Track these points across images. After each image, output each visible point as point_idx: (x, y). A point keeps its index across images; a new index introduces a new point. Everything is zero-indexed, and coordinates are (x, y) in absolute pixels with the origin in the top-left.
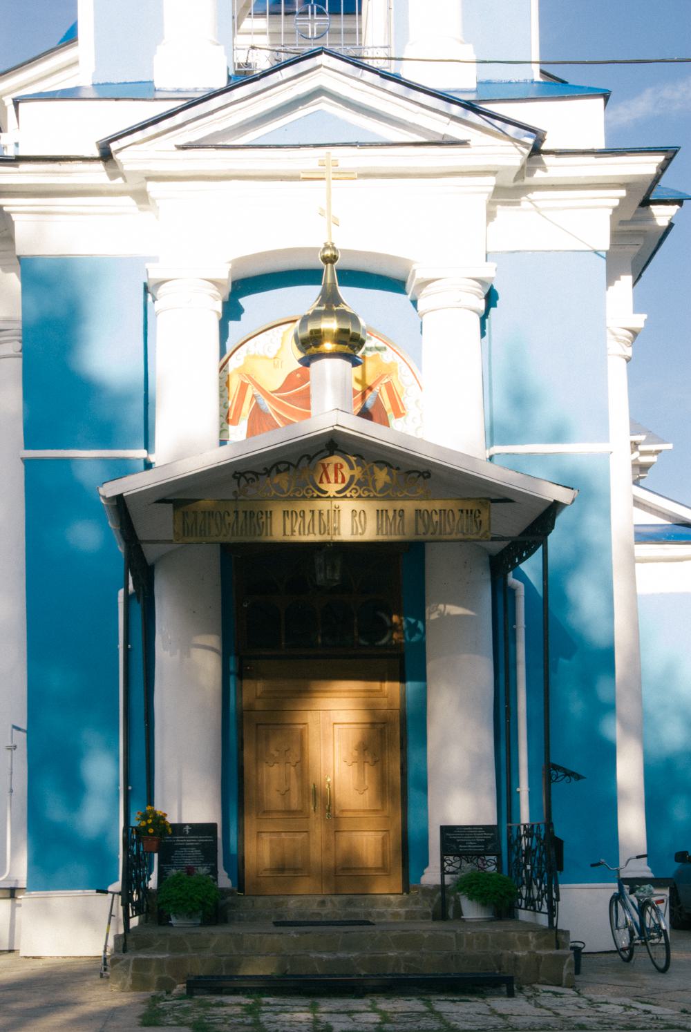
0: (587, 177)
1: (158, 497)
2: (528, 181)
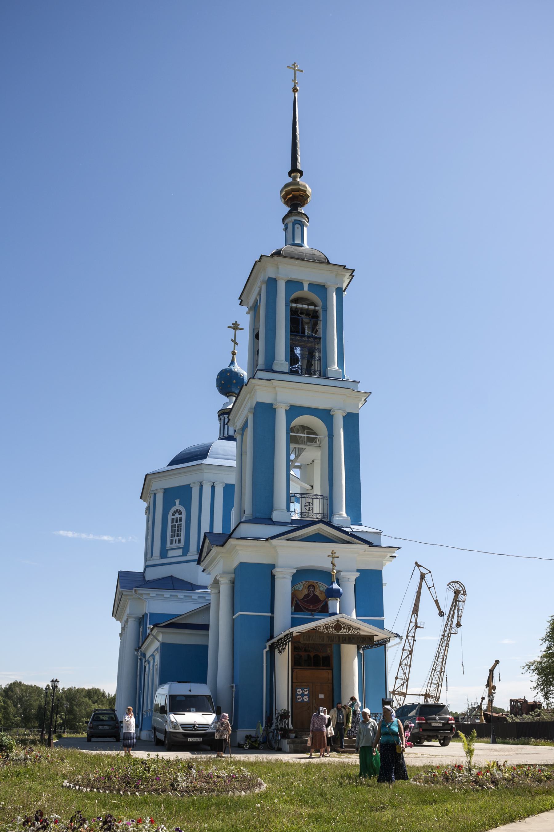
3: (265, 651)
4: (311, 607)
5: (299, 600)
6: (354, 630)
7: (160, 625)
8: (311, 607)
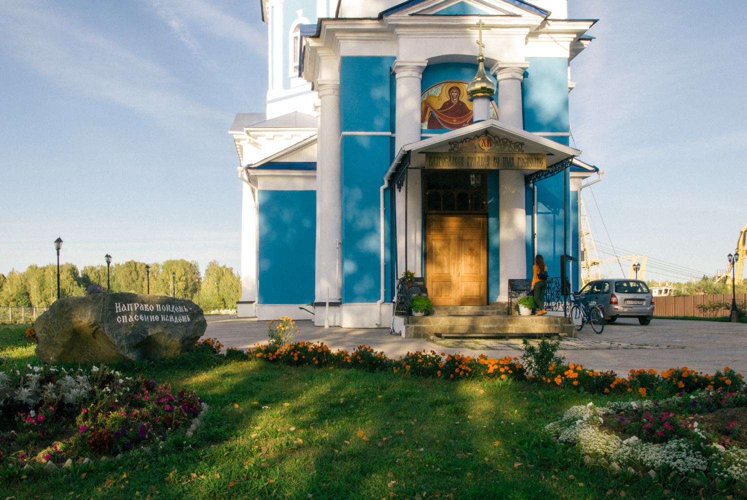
0: (563, 30)
1: (418, 152)
2: (540, 30)
3: (382, 188)
4: (455, 122)
5: (436, 111)
6: (512, 145)
7: (253, 166)
8: (455, 121)
